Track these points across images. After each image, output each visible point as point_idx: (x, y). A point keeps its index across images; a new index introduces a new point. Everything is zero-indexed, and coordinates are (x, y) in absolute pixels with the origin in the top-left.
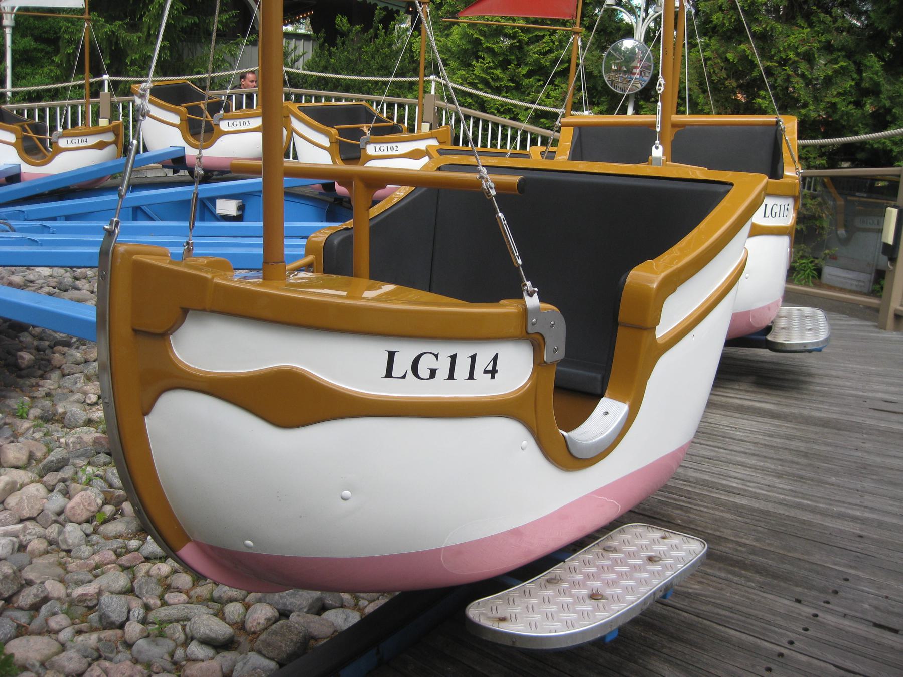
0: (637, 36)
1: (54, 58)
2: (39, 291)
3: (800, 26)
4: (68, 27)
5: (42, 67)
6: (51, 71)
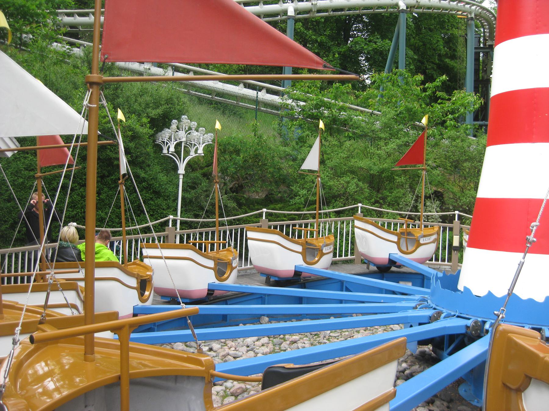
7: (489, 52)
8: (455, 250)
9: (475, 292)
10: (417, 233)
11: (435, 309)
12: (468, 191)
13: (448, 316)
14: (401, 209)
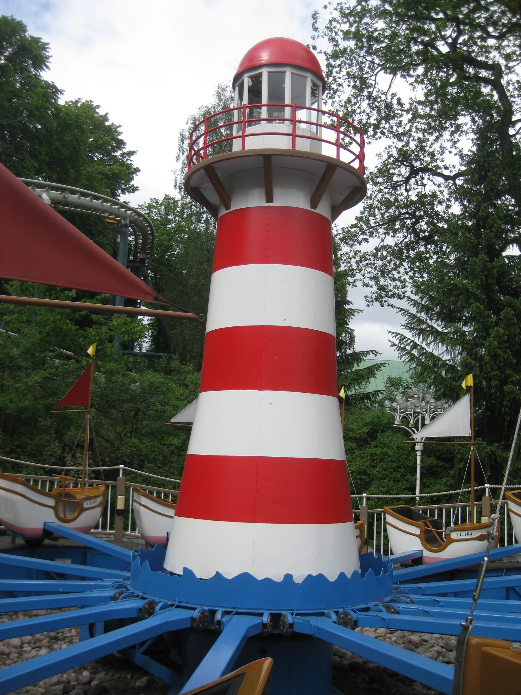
1: (449, 471)
2: (431, 649)
4: (460, 450)
5: (442, 478)
6: (448, 481)
7: (140, 267)
8: (119, 515)
9: (199, 574)
10: (80, 494)
11: (143, 598)
12: (129, 439)
13: (164, 607)
14: (44, 462)
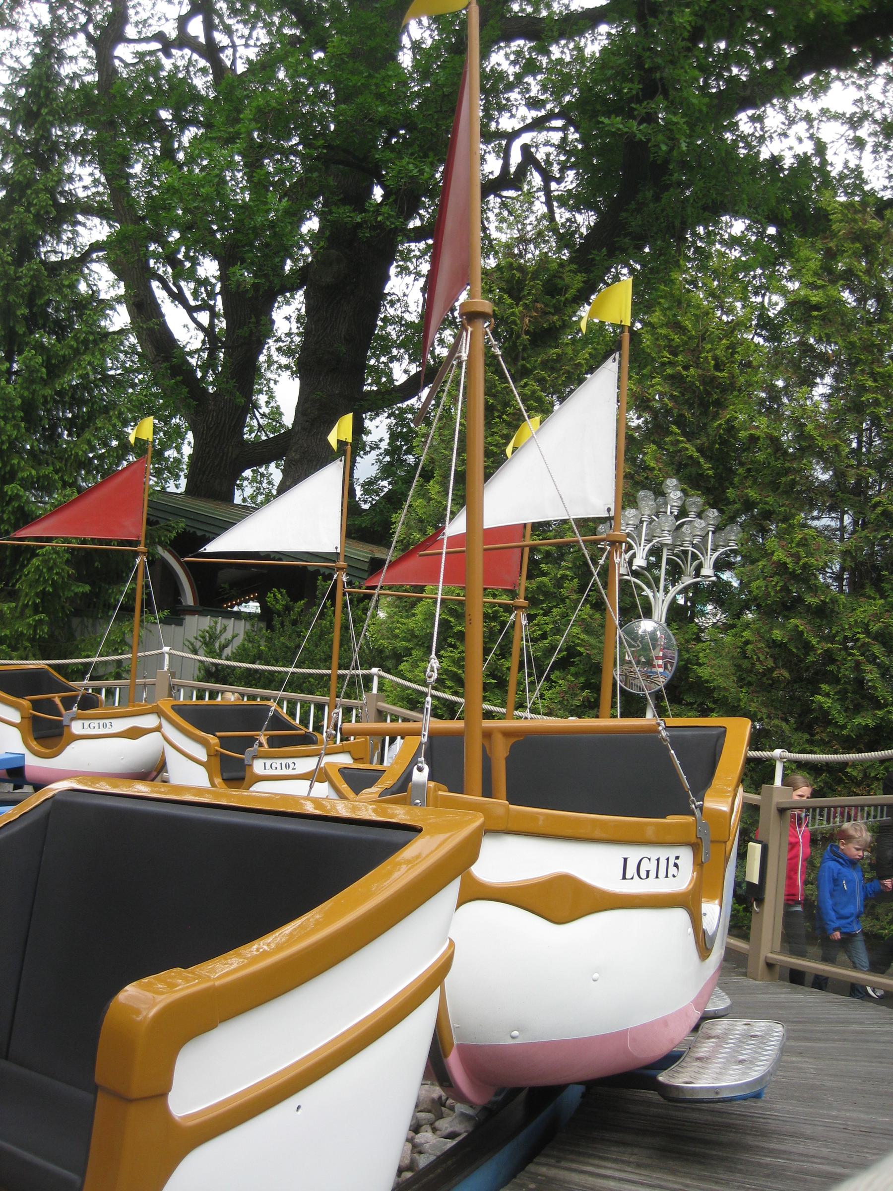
0: (656, 614)
3: (869, 597)
